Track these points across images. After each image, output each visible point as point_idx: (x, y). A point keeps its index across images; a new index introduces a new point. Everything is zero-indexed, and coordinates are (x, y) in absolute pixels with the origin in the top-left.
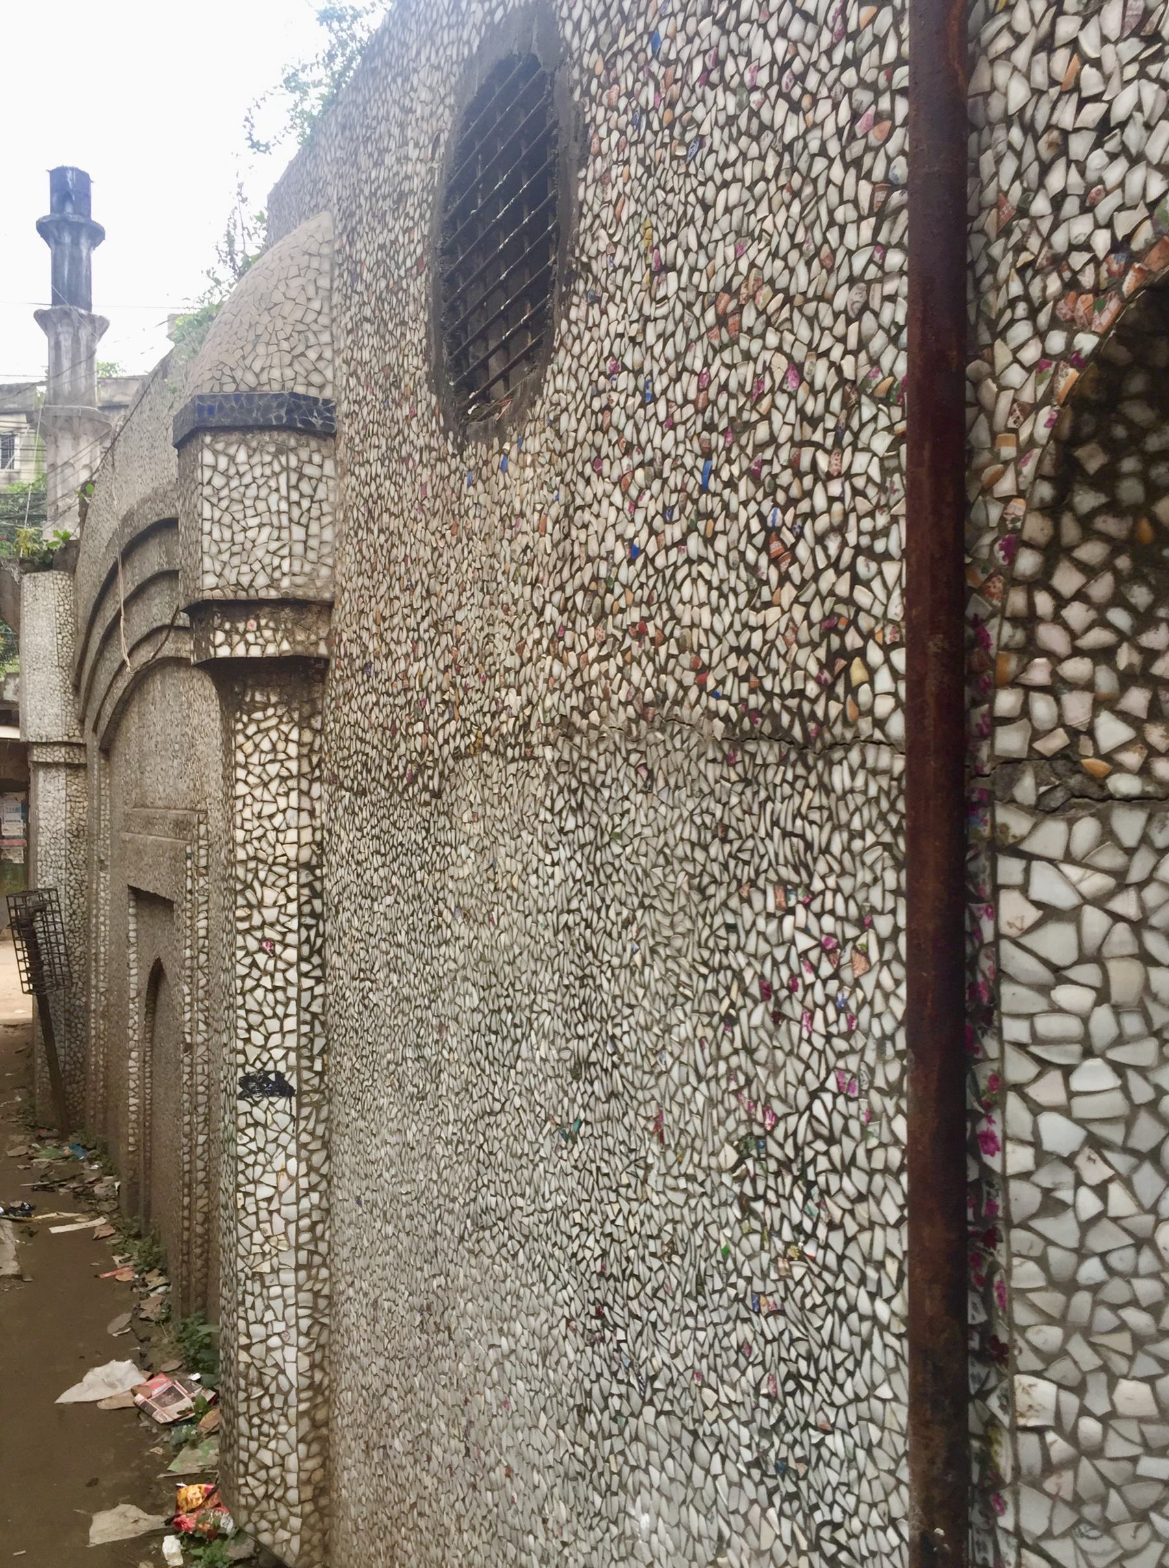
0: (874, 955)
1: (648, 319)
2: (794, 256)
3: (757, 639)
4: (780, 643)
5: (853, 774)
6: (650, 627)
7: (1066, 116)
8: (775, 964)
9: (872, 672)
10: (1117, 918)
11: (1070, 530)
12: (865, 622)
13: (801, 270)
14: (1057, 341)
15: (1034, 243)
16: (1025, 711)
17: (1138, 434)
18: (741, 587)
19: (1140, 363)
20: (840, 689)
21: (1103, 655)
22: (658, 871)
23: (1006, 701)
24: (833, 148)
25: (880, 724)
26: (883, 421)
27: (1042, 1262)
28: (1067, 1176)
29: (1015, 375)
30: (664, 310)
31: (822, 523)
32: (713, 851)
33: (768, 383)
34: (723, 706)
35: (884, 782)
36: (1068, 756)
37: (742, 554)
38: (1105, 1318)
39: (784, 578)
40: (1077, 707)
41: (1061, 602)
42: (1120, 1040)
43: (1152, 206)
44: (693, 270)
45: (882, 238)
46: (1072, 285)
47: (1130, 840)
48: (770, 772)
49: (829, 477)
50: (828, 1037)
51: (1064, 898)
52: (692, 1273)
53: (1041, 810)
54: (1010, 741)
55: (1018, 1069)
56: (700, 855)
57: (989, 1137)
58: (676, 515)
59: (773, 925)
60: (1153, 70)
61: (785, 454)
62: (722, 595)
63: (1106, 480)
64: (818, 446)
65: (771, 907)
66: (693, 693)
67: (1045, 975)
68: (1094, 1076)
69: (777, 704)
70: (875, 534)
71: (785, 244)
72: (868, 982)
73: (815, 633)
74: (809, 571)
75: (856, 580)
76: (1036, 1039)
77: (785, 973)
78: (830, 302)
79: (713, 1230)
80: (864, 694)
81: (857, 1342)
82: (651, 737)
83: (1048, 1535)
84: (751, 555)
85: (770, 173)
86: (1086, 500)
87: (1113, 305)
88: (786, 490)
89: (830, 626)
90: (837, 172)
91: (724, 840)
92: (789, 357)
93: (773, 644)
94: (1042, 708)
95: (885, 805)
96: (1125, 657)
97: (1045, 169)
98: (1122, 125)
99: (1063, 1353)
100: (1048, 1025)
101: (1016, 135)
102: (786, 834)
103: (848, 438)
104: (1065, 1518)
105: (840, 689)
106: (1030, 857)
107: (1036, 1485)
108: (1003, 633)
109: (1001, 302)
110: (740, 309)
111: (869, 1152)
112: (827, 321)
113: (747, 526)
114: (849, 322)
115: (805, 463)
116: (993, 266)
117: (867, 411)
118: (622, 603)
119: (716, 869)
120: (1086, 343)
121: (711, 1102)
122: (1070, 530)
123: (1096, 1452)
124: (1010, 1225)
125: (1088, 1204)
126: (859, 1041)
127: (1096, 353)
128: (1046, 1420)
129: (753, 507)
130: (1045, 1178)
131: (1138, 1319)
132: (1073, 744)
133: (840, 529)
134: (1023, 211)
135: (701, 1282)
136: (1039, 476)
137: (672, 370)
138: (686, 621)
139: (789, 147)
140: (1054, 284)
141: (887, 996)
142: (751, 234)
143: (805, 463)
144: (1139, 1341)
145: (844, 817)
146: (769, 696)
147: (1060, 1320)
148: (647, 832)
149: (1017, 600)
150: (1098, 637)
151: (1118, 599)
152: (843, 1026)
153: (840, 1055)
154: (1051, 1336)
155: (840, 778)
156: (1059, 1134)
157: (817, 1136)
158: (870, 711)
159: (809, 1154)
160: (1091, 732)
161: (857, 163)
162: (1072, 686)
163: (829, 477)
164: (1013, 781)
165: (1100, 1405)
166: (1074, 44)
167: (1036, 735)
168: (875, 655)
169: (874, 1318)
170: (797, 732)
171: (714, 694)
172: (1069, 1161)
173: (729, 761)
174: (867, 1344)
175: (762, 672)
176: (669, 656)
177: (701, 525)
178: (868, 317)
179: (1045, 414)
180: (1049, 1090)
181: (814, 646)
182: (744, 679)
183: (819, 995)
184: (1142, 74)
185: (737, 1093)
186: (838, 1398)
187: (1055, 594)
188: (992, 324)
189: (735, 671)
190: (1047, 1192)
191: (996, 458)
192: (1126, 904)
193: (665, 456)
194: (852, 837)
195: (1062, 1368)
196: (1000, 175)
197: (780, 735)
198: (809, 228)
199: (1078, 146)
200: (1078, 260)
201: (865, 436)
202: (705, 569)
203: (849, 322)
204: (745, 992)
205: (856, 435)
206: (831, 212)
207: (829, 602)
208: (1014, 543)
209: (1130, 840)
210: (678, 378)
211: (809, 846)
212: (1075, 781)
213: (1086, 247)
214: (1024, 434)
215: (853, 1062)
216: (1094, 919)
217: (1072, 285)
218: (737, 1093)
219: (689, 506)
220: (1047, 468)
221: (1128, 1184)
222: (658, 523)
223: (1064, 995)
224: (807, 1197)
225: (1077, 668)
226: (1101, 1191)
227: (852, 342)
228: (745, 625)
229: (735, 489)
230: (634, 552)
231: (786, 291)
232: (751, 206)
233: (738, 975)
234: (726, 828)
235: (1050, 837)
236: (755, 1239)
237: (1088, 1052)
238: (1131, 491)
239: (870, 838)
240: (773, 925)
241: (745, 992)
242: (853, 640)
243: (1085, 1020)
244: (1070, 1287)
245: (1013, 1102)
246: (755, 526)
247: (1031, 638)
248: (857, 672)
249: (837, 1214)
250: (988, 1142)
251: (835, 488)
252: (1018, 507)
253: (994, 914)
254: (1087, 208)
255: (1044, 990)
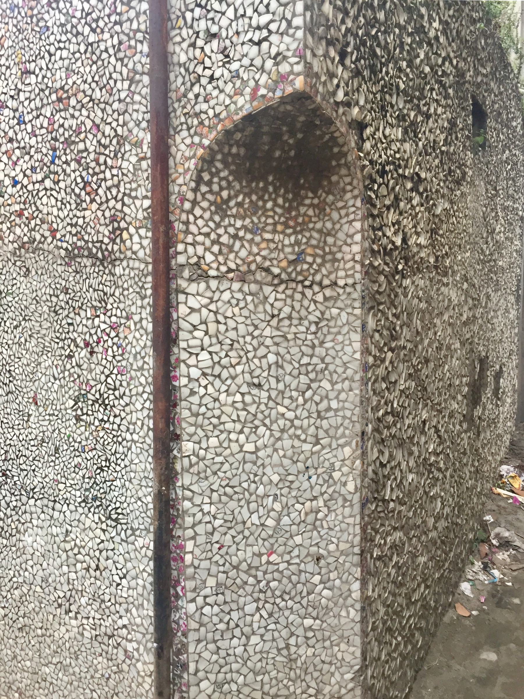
0: (133, 327)
1: (20, 90)
2: (94, 85)
3: (80, 221)
4: (92, 224)
5: (124, 269)
6: (26, 213)
7: (199, 70)
8: (91, 335)
9: (131, 236)
10: (210, 311)
11: (199, 198)
12: (128, 219)
13: (97, 90)
14: (197, 139)
15: (189, 107)
16: (186, 251)
17: (218, 171)
18: (72, 202)
19: (220, 151)
20: (118, 240)
21: (207, 235)
22: (33, 306)
23: (180, 247)
24: (111, 51)
25: (134, 253)
26: (134, 152)
27: (190, 409)
28: (197, 384)
29: (182, 147)
30: (29, 88)
31: (109, 183)
32: (61, 297)
33: (83, 129)
34: (65, 245)
35: (137, 272)
36: (197, 264)
37: (73, 190)
38: (206, 422)
39: (93, 201)
40: (200, 250)
41: (196, 218)
42: (211, 345)
43: (227, 106)
44: (44, 77)
45: (132, 89)
46: (201, 123)
47: (214, 289)
48: (88, 269)
49: (112, 167)
50: (114, 357)
51: (197, 306)
52: (53, 448)
53: (190, 280)
54: (181, 259)
55: (184, 355)
56: (54, 299)
57: (175, 376)
58: (38, 170)
59: (90, 321)
60: (227, 66)
61: (92, 156)
62: (62, 203)
63: (209, 183)
64: (107, 156)
65: (89, 315)
66: (50, 240)
67: (191, 328)
68: (204, 356)
69: (90, 245)
70: (131, 190)
71: (90, 80)
72: (130, 337)
73: (107, 221)
74: (104, 199)
75: (124, 204)
76: (189, 347)
77: (95, 338)
78: (111, 106)
79: (63, 430)
80: (128, 243)
81: (126, 450)
82: (27, 255)
83: (191, 484)
84: (77, 191)
85: (82, 51)
86: (204, 189)
87: (214, 133)
88: (93, 169)
89: (113, 219)
90: (113, 60)
91: (66, 293)
92: (93, 121)
93: (88, 224)
94: (190, 249)
95: (137, 279)
96: (213, 236)
97: (193, 85)
98: (218, 79)
99: (195, 433)
100: (192, 342)
101: (182, 70)
102: (95, 290)
103: (120, 155)
104: (195, 478)
105: (118, 240)
106: (187, 294)
107: (188, 471)
108: (178, 226)
109: (178, 122)
110: (69, 98)
111: (130, 390)
112: (110, 112)
113: (75, 179)
114: (119, 115)
115: (102, 160)
116: (175, 110)
117: (128, 147)
118: (9, 202)
119: (63, 304)
120: (206, 142)
121: (61, 386)
122: (199, 198)
123: (204, 459)
124: (181, 400)
125: (202, 391)
126: (126, 356)
127: (209, 146)
128: (191, 453)
129: (77, 173)
130: (190, 386)
131: (215, 421)
132: (199, 261)
133: (117, 186)
134: (185, 96)
135: (57, 450)
136: (191, 180)
137: (34, 113)
138: (45, 211)
139: (91, 44)
140: (196, 122)
141: (137, 340)
142: (74, 71)
143: (102, 160)
144: (215, 427)
145: (120, 283)
146: (87, 242)
147: (195, 425)
148: (26, 292)
149: (184, 217)
150: (206, 230)
151: (211, 219)
152: (120, 352)
153: (118, 362)
154: (192, 429)
155: (118, 271)
156: (195, 373)
157: (109, 389)
158: (131, 249)
159: (106, 396)
160: (204, 258)
161: (122, 60)
162: (199, 244)
163: (112, 167)
164: (182, 272)
165: (204, 445)
166: (202, 49)
167: (189, 258)
168: (132, 230)
169: (132, 440)
170: (100, 255)
171: (60, 240)
172: (197, 380)
173: (68, 265)
174: (129, 449)
175: (83, 233)
176: (36, 225)
177: (52, 176)
178: (127, 115)
179: (193, 161)
180: (192, 361)
181: (107, 225)
182: (76, 235)
183: (110, 343)
184: (223, 66)
185: (73, 381)
186: (118, 468)
187: (195, 216)
188: (175, 129)
189: (70, 233)
190: (191, 390)
191: (177, 171)
192: (213, 307)
193: (31, 147)
194: (124, 290)
195: (196, 438)
196: (177, 81)
197: (91, 255)
198: (101, 77)
199: (204, 81)
200: (203, 116)
201: (126, 156)
202: (54, 193)
203: (119, 115)
204: (77, 346)
205: (123, 155)
206: (110, 74)
207: (113, 211)
208: (183, 199)
209: (214, 289)
210: (38, 117)
211: (105, 294)
212: (199, 272)
213: (206, 113)
214: (186, 166)
215: (124, 363)
216: (204, 311)
217: (201, 123)
218: (73, 381)
219: (45, 168)
220: (194, 178)
221: (212, 384)
222: (28, 172)
223: (196, 334)
224: (105, 409)
225: (200, 238)
226: (206, 387)
227: (121, 122)
228: (75, 216)
229: (69, 165)
230: (15, 183)
231: (91, 96)
232: (73, 61)
233: (74, 340)
234: (67, 289)
235: (193, 288)
236: (83, 429)
237: (203, 349)
238: (216, 188)
239: (131, 290)
240: (90, 321)
241: (77, 346)
242: (123, 225)
243: (202, 340)
244: (197, 415)
245: (182, 365)
246: (79, 180)
247: (187, 229)
248: (125, 235)
249: (117, 412)
250: (175, 378)
251: (115, 171)
252: (184, 188)
253: (177, 311)
254: (206, 101)
255: (191, 332)
